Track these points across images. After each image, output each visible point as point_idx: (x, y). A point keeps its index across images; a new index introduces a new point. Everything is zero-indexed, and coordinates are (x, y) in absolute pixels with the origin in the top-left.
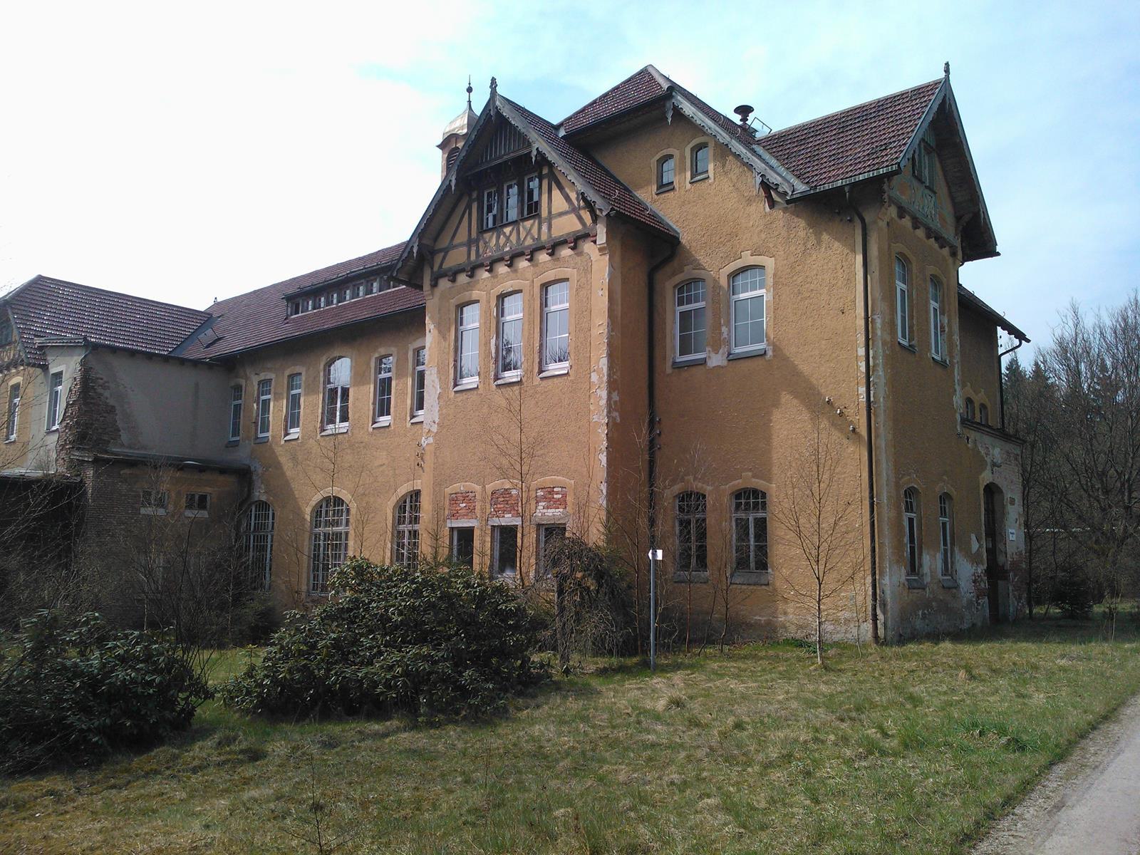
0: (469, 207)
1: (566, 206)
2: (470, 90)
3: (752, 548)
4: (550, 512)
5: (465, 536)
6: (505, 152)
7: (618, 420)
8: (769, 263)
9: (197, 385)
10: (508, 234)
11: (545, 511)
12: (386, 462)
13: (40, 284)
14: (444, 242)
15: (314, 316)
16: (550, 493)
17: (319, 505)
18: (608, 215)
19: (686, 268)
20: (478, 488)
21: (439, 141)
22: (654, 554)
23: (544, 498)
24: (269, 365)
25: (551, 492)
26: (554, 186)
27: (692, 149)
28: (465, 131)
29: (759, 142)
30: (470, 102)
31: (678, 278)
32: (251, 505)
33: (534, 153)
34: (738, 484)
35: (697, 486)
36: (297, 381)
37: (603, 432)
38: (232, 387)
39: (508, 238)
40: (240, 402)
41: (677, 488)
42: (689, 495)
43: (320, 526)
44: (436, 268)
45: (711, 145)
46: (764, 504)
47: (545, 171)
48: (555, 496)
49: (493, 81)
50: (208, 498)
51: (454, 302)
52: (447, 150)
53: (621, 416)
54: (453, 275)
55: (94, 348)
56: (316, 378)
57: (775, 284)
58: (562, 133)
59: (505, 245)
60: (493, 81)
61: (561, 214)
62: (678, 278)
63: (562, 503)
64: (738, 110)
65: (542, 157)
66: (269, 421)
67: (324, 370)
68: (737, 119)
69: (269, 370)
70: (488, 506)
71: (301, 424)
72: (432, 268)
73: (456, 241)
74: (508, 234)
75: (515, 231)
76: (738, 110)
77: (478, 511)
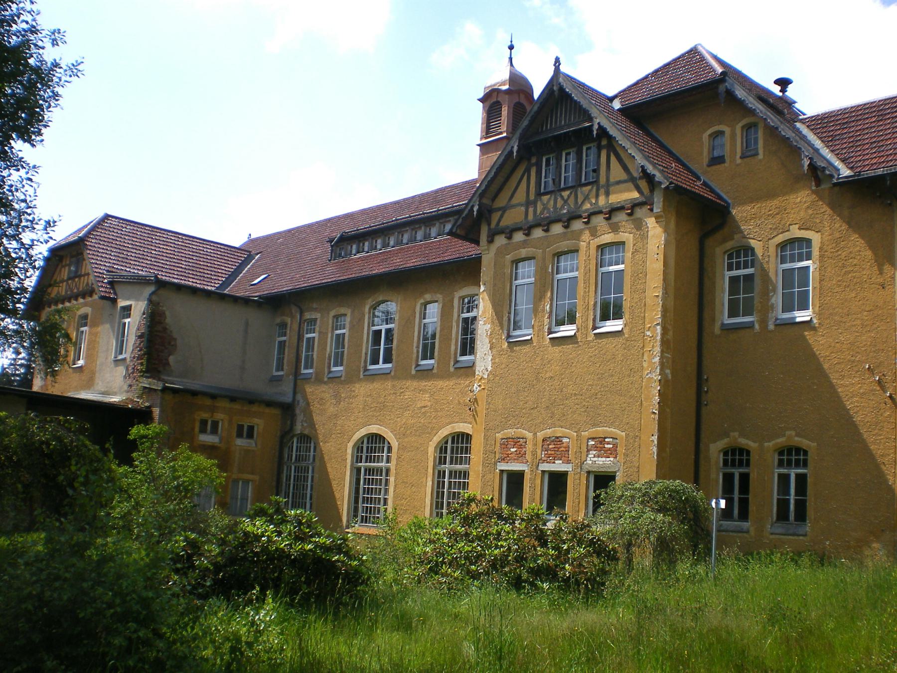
0: (528, 171)
1: (623, 176)
2: (511, 48)
3: (792, 502)
4: (601, 461)
5: (515, 481)
6: (564, 125)
7: (670, 376)
8: (815, 238)
9: (247, 324)
10: (566, 197)
11: (596, 459)
12: (429, 404)
13: (107, 217)
14: (501, 202)
15: (364, 262)
16: (601, 443)
17: (361, 441)
18: (667, 188)
19: (736, 237)
20: (529, 435)
21: (481, 95)
22: (717, 503)
23: (595, 447)
24: (315, 306)
25: (602, 440)
26: (613, 158)
27: (743, 127)
28: (506, 87)
29: (802, 121)
30: (511, 59)
31: (729, 245)
32: (292, 437)
33: (596, 127)
34: (781, 441)
35: (743, 442)
36: (341, 320)
37: (655, 388)
38: (277, 325)
39: (566, 202)
40: (284, 338)
41: (722, 444)
42: (734, 451)
43: (382, 462)
44: (493, 226)
45: (761, 126)
46: (748, 461)
47: (604, 142)
48: (606, 446)
49: (557, 60)
50: (256, 429)
51: (509, 258)
52: (488, 104)
53: (672, 373)
54: (509, 233)
55: (161, 284)
56: (361, 320)
57: (822, 257)
58: (617, 105)
59: (562, 208)
60: (557, 60)
61: (619, 183)
62: (729, 245)
63: (613, 452)
64: (777, 82)
65: (602, 131)
66: (312, 359)
67: (369, 313)
68: (776, 90)
69: (316, 310)
70: (539, 451)
71: (345, 363)
72: (489, 225)
73: (514, 201)
74: (566, 197)
75: (573, 195)
76: (777, 82)
77: (529, 457)
